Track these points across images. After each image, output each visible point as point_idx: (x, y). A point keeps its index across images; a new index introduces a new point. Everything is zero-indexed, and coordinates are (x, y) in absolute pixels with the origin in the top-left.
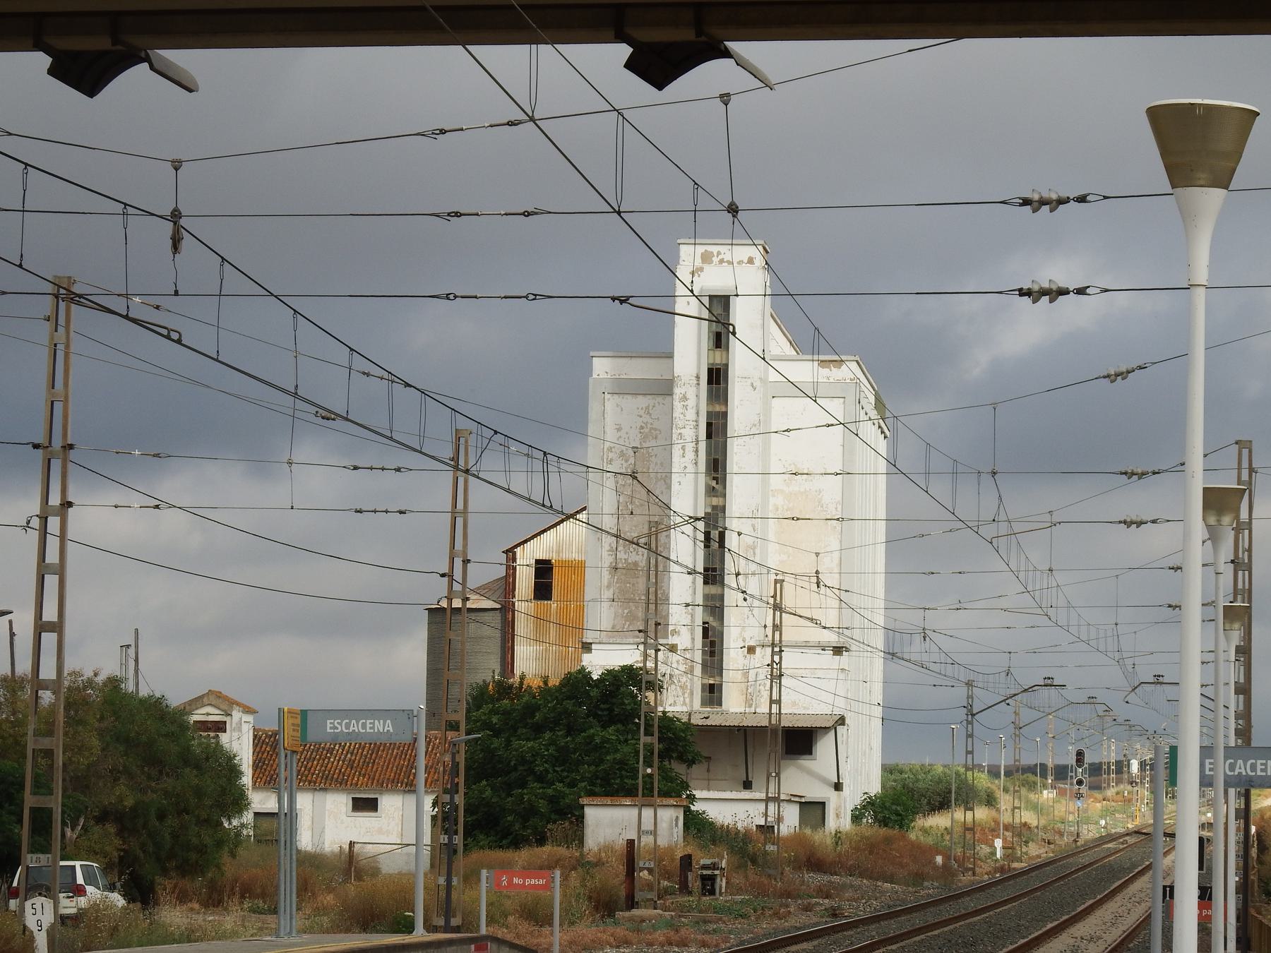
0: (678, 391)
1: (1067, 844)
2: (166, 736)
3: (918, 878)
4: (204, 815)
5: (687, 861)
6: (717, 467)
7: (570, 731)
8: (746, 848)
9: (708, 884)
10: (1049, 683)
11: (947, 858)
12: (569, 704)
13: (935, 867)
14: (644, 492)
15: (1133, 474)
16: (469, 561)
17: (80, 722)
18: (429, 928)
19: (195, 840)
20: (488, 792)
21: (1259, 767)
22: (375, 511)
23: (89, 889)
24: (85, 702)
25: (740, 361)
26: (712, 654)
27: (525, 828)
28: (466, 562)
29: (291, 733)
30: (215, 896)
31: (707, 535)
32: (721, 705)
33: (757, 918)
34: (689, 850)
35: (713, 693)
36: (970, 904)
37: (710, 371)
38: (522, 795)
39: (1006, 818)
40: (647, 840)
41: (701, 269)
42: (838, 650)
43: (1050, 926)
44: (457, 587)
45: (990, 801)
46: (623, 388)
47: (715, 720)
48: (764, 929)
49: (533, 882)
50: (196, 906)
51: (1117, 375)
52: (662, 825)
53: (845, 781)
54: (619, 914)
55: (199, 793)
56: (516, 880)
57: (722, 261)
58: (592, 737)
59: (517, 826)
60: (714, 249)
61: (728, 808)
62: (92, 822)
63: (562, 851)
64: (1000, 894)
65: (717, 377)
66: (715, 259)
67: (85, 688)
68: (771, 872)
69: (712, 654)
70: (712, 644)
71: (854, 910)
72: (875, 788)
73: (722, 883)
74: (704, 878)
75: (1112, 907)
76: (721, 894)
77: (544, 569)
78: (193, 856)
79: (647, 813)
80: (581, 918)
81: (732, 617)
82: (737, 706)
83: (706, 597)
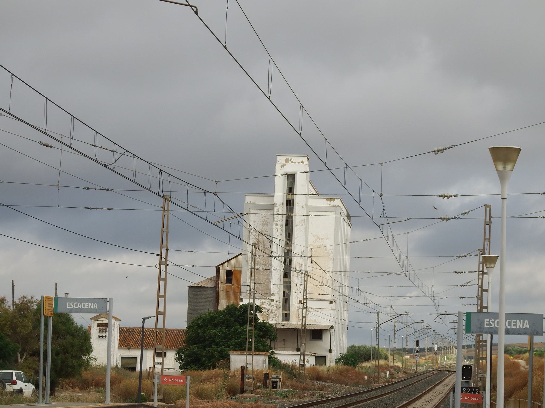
0: (276, 208)
1: (412, 373)
2: (60, 323)
3: (357, 384)
4: (74, 354)
5: (266, 376)
6: (289, 236)
7: (228, 327)
8: (289, 370)
9: (275, 384)
10: (407, 314)
11: (369, 377)
12: (228, 317)
13: (364, 380)
14: (222, 204)
15: (445, 196)
16: (168, 249)
17: (25, 316)
18: (112, 400)
19: (70, 364)
20: (196, 349)
21: (513, 324)
22: (97, 209)
23: (18, 381)
24: (27, 309)
25: (299, 199)
26: (286, 302)
27: (209, 362)
28: (167, 250)
29: (47, 308)
30: (85, 386)
31: (285, 260)
32: (289, 320)
33: (292, 398)
34: (269, 372)
35: (286, 317)
36: (375, 394)
37: (287, 201)
38: (209, 350)
39: (391, 364)
40: (250, 367)
41: (285, 165)
42: (331, 302)
43: (405, 403)
44: (163, 260)
45: (386, 358)
46: (258, 207)
47: (286, 326)
48: (295, 401)
49: (474, 399)
50: (77, 389)
51: (439, 151)
52: (259, 362)
53: (333, 349)
54: (238, 395)
55: (72, 345)
56: (466, 398)
57: (292, 162)
58: (237, 329)
59: (207, 362)
60: (290, 158)
61: (287, 357)
62: (28, 356)
63: (221, 371)
64: (386, 390)
65: (290, 204)
66: (290, 161)
67: (27, 303)
68: (301, 381)
69: (286, 302)
70: (286, 299)
71: (330, 395)
72: (344, 352)
73: (280, 384)
74: (273, 382)
75: (429, 396)
76: (279, 388)
77: (229, 273)
78: (70, 370)
79: (250, 358)
80: (223, 396)
81: (293, 289)
82: (294, 322)
83: (284, 282)
